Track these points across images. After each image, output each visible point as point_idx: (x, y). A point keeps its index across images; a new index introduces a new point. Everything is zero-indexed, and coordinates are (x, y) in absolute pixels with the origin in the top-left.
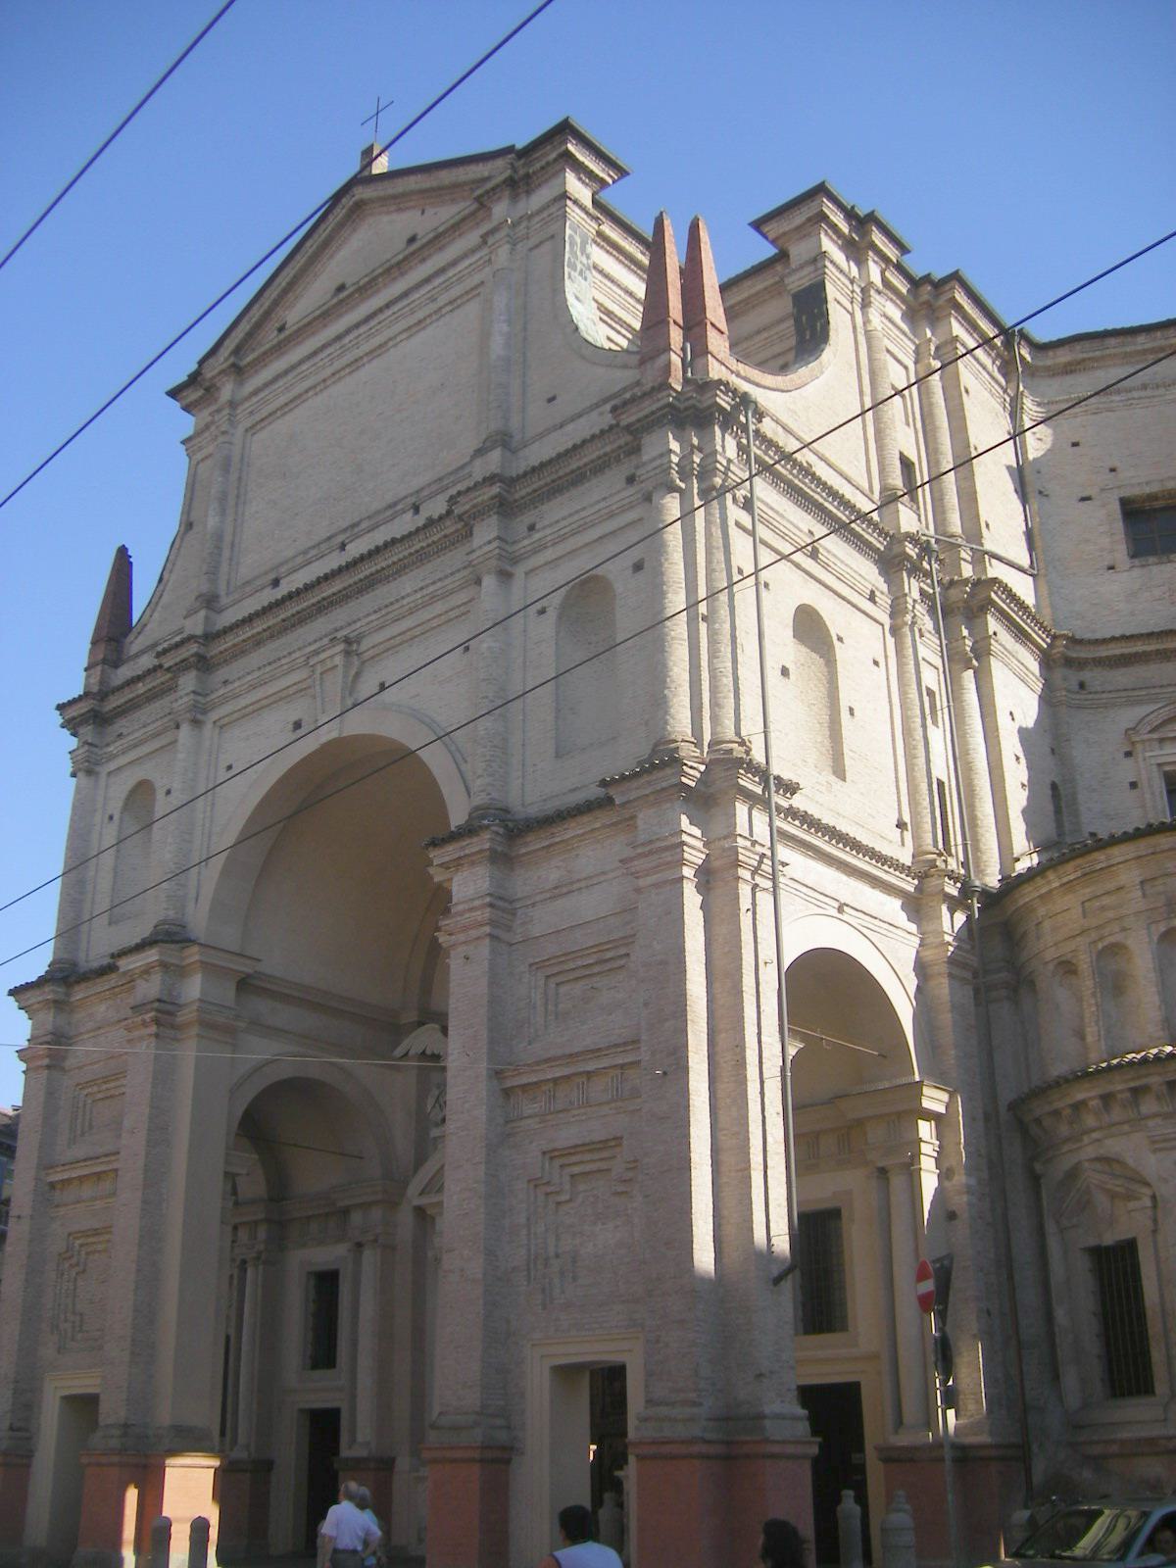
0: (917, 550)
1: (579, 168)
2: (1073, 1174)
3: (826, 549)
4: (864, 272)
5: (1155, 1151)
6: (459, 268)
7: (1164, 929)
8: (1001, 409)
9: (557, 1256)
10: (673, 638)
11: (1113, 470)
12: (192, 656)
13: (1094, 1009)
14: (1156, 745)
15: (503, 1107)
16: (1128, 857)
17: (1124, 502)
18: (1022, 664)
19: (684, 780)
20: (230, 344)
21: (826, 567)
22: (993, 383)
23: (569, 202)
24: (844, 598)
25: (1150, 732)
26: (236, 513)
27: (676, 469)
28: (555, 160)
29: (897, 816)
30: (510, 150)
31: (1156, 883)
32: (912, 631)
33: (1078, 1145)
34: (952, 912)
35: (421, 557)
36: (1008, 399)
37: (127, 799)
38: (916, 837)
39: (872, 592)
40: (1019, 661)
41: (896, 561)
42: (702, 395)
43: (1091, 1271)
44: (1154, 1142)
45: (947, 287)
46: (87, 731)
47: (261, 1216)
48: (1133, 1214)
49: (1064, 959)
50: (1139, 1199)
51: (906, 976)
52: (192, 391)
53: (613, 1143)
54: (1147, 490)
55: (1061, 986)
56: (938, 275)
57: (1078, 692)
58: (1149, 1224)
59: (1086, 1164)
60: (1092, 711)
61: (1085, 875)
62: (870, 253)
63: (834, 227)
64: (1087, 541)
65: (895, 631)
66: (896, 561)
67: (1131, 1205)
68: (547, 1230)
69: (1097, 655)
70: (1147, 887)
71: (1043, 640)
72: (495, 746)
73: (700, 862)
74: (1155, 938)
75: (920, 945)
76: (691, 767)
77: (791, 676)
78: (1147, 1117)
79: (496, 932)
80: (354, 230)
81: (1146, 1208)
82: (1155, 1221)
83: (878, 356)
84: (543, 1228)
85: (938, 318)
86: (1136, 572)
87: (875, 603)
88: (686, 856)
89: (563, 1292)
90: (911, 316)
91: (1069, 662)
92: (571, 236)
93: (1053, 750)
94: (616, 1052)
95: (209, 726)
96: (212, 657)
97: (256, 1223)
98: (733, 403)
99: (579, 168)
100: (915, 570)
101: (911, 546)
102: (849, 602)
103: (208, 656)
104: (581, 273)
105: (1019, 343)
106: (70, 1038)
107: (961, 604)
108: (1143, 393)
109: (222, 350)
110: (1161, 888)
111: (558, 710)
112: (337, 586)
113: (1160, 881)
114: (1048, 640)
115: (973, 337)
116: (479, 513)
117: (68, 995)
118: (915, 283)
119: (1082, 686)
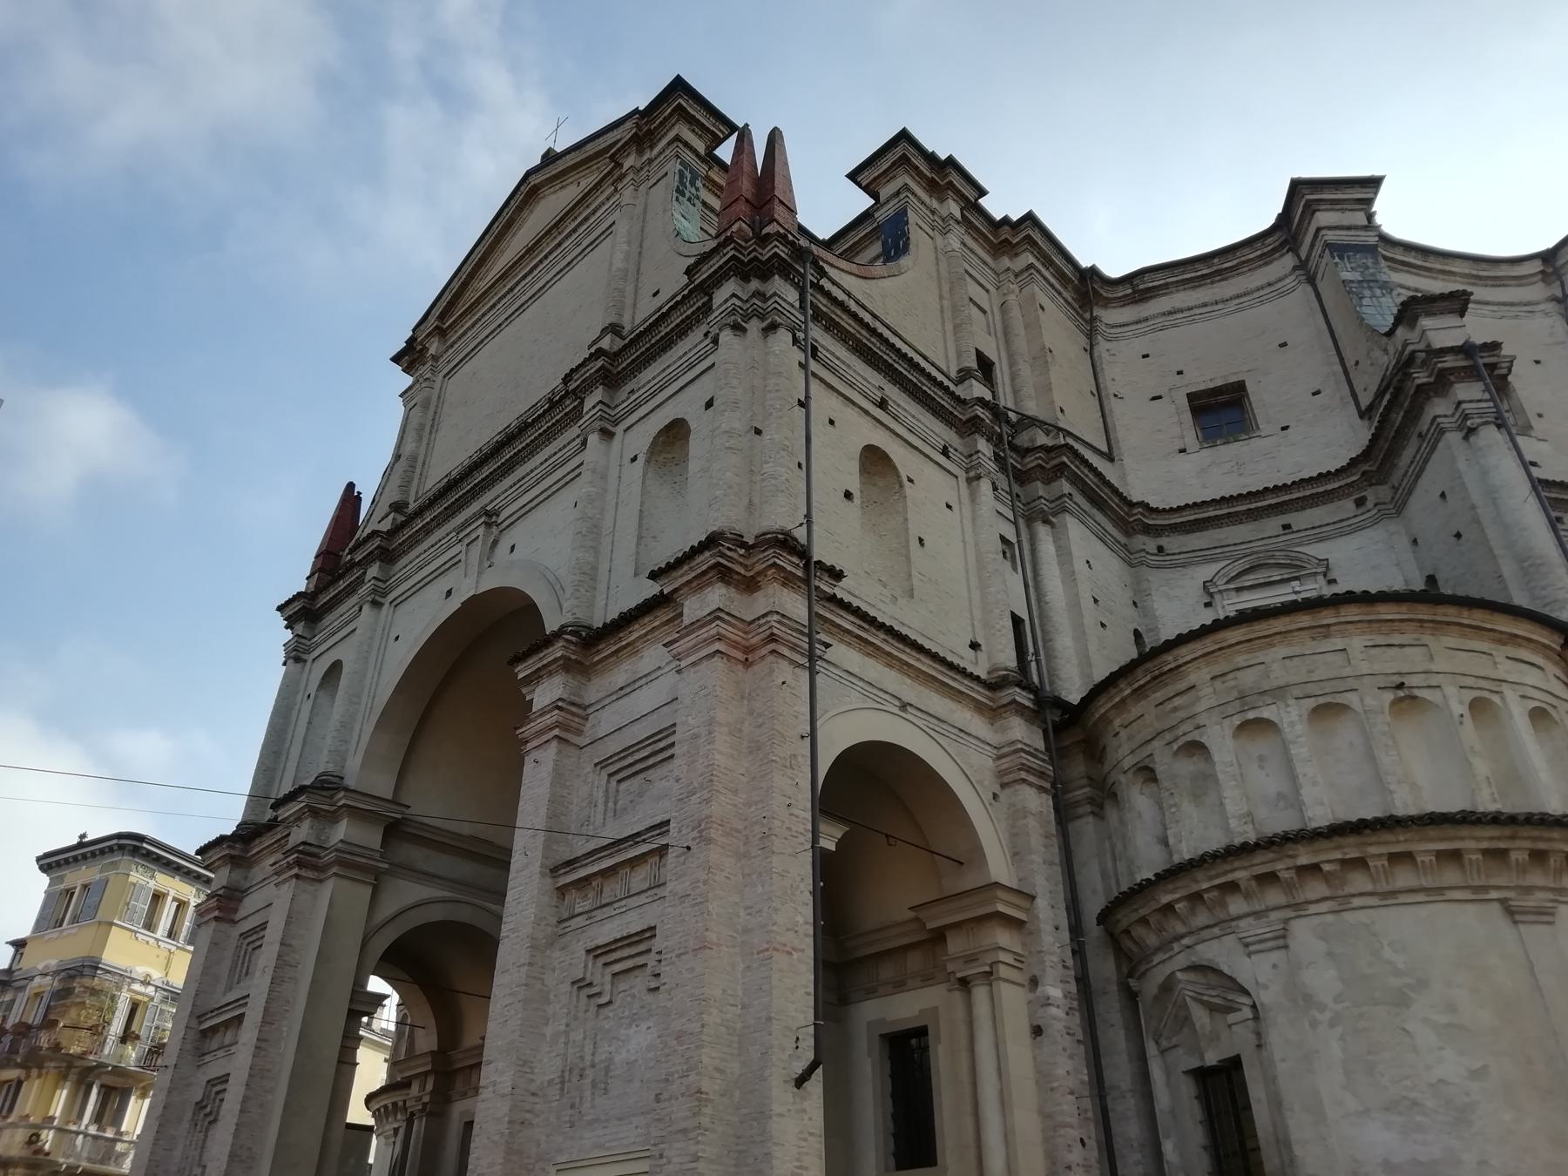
2: (1168, 986)
3: (895, 402)
6: (598, 214)
7: (1239, 723)
9: (593, 1066)
11: (1180, 373)
12: (376, 548)
15: (557, 907)
20: (437, 312)
24: (916, 448)
25: (1227, 583)
33: (1171, 953)
35: (548, 436)
37: (323, 679)
39: (945, 448)
40: (1095, 521)
43: (1196, 1097)
46: (300, 628)
47: (429, 1067)
48: (1233, 1027)
49: (1141, 765)
51: (980, 782)
52: (409, 357)
53: (647, 935)
54: (1211, 385)
55: (1142, 794)
57: (1156, 555)
58: (1252, 1038)
59: (1179, 975)
62: (950, 192)
67: (1231, 1018)
68: (584, 1039)
72: (583, 573)
77: (855, 499)
78: (1239, 918)
79: (564, 735)
80: (532, 212)
81: (1248, 1019)
82: (1258, 1035)
84: (582, 1036)
86: (1205, 453)
87: (948, 457)
89: (593, 1107)
93: (1135, 603)
94: (653, 836)
95: (387, 605)
97: (426, 1074)
104: (689, 200)
110: (1233, 683)
111: (640, 537)
112: (486, 471)
113: (1231, 676)
116: (587, 387)
119: (1160, 549)
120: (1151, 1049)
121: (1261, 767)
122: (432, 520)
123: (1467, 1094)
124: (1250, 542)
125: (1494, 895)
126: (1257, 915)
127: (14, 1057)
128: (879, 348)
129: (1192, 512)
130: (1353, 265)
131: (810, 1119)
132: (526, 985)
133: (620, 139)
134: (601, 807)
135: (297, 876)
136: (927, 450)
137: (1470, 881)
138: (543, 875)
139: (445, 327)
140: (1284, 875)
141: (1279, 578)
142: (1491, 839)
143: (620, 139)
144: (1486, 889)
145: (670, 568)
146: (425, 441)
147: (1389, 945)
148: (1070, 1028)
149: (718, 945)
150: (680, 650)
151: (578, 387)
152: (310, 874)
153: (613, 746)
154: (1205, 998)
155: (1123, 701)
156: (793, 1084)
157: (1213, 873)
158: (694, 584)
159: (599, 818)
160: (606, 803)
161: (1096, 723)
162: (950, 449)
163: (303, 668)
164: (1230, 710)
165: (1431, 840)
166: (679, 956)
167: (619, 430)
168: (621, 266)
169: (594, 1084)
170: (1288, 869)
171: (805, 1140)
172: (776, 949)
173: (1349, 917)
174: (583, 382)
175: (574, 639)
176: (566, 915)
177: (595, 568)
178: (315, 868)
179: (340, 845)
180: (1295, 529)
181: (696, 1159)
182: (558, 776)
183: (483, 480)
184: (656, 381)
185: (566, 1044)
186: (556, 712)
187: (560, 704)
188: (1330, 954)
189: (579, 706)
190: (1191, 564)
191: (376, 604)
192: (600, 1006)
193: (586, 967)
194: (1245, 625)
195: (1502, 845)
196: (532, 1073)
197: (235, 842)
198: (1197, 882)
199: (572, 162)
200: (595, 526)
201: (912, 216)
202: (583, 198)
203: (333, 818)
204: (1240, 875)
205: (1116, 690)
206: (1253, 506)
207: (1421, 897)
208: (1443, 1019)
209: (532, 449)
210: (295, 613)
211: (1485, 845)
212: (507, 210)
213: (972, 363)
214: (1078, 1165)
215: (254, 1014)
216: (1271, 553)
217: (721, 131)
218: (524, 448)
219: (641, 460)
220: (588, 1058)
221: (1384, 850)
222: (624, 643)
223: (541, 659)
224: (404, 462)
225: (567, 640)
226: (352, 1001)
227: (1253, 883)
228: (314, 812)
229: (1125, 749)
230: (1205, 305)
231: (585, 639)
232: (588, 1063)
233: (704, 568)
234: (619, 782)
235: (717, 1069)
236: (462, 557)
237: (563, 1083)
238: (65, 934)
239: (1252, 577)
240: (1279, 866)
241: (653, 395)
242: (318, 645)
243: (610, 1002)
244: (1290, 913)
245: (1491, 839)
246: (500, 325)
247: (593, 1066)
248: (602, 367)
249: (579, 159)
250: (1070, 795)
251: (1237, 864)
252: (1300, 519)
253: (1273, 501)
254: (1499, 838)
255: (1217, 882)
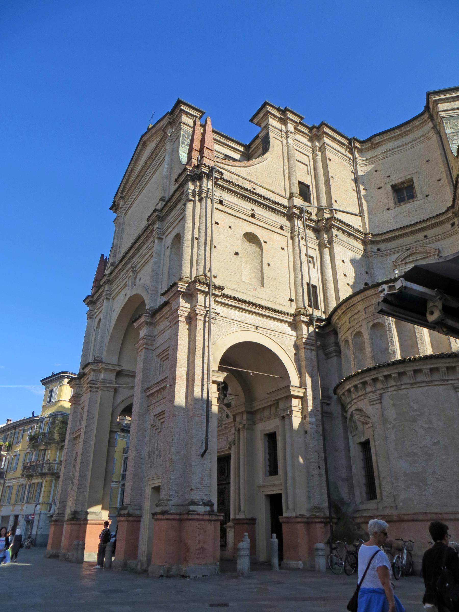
0: (299, 211)
1: (187, 113)
2: (352, 415)
3: (258, 214)
4: (287, 127)
5: (370, 405)
8: (349, 165)
10: (186, 246)
13: (353, 355)
14: (404, 265)
16: (359, 300)
17: (393, 187)
18: (350, 244)
19: (179, 289)
20: (120, 191)
21: (259, 220)
22: (343, 156)
23: (182, 124)
25: (402, 261)
26: (121, 239)
27: (191, 194)
28: (179, 113)
29: (290, 297)
30: (168, 113)
31: (369, 308)
32: (298, 237)
33: (351, 405)
34: (308, 327)
36: (351, 161)
38: (297, 303)
41: (292, 215)
42: (198, 170)
44: (370, 402)
45: (321, 128)
50: (369, 423)
51: (289, 350)
54: (400, 181)
56: (317, 125)
60: (383, 257)
61: (348, 309)
63: (273, 115)
64: (380, 202)
65: (292, 238)
66: (292, 215)
69: (383, 238)
70: (366, 310)
71: (361, 236)
73: (186, 315)
74: (370, 327)
75: (296, 339)
76: (182, 285)
79: (148, 347)
80: (145, 151)
83: (292, 153)
85: (320, 139)
86: (397, 209)
87: (283, 230)
88: (179, 313)
89: (156, 462)
90: (311, 140)
91: (373, 242)
92: (183, 135)
95: (111, 299)
96: (111, 280)
98: (209, 170)
99: (187, 113)
100: (300, 217)
101: (296, 210)
102: (270, 230)
103: (110, 279)
105: (354, 142)
106: (81, 395)
107: (323, 227)
108: (398, 149)
109: (118, 193)
114: (363, 236)
115: (335, 143)
117: (80, 382)
118: (311, 129)
119: (378, 250)
120: (350, 436)
121: (381, 339)
122: (120, 269)
123: (432, 450)
124: (412, 244)
125: (450, 382)
126: (373, 392)
127: (42, 442)
128: (250, 195)
129: (390, 234)
130: (451, 126)
131: (206, 466)
132: (138, 427)
133: (164, 124)
134: (158, 370)
135: (90, 391)
136: (273, 229)
137: (442, 378)
138: (142, 392)
139: (123, 196)
140: (381, 378)
141: (420, 258)
142: (450, 363)
143: (164, 124)
144: (447, 380)
145: (166, 292)
146: (120, 239)
147: (412, 401)
148: (317, 431)
149: (178, 416)
150: (170, 320)
151: (151, 222)
152: (94, 390)
153: (161, 350)
154: (360, 420)
155: (340, 316)
156: (200, 456)
157: (359, 378)
158: (174, 297)
159: (158, 373)
160: (160, 368)
161: (334, 324)
162: (283, 227)
163: (93, 320)
164: (370, 320)
165: (427, 364)
166: (168, 419)
167: (164, 237)
168: (165, 174)
169: (157, 456)
170: (381, 376)
171: (205, 472)
172: (194, 416)
173: (401, 392)
174: (153, 220)
175: (148, 315)
176: (150, 404)
177: (157, 288)
178: (96, 388)
179: (102, 380)
180: (429, 237)
181: (170, 479)
182: (146, 360)
183: (132, 255)
184: (172, 219)
185: (150, 444)
186: (143, 340)
187: (145, 337)
188: (394, 405)
189: (152, 336)
190: (389, 254)
191: (108, 299)
192: (159, 432)
193: (154, 420)
194: (374, 288)
195: (454, 365)
196: (141, 452)
197: (77, 380)
198: (355, 381)
199: (153, 132)
200: (157, 273)
201: (271, 135)
202: (157, 146)
203: (99, 371)
204: (367, 379)
205: (337, 313)
206: (412, 229)
207: (424, 384)
208: (426, 426)
209: (143, 244)
210: (88, 302)
211: (447, 365)
212: (137, 151)
213: (296, 189)
214: (316, 475)
215: (82, 433)
216: (418, 248)
217: (198, 114)
218: (141, 244)
219: (169, 248)
220: (156, 448)
221: (412, 369)
222: (162, 315)
223: (140, 322)
224: (114, 249)
225: (145, 316)
226: (111, 428)
227: (371, 381)
228: (94, 370)
229: (342, 334)
230: (399, 147)
231: (151, 315)
232: (156, 449)
233: (175, 292)
234: (164, 361)
235: (177, 453)
236: (127, 283)
237: (149, 455)
238: (52, 404)
239: (411, 258)
240: (378, 375)
241: (172, 224)
242: (96, 313)
243: (160, 431)
244: (383, 391)
245: (450, 363)
246: (137, 195)
247: (157, 450)
248: (157, 215)
249: (155, 131)
250: (327, 351)
251: (366, 375)
252: (429, 233)
253: (420, 227)
254: (452, 362)
255: (361, 381)
